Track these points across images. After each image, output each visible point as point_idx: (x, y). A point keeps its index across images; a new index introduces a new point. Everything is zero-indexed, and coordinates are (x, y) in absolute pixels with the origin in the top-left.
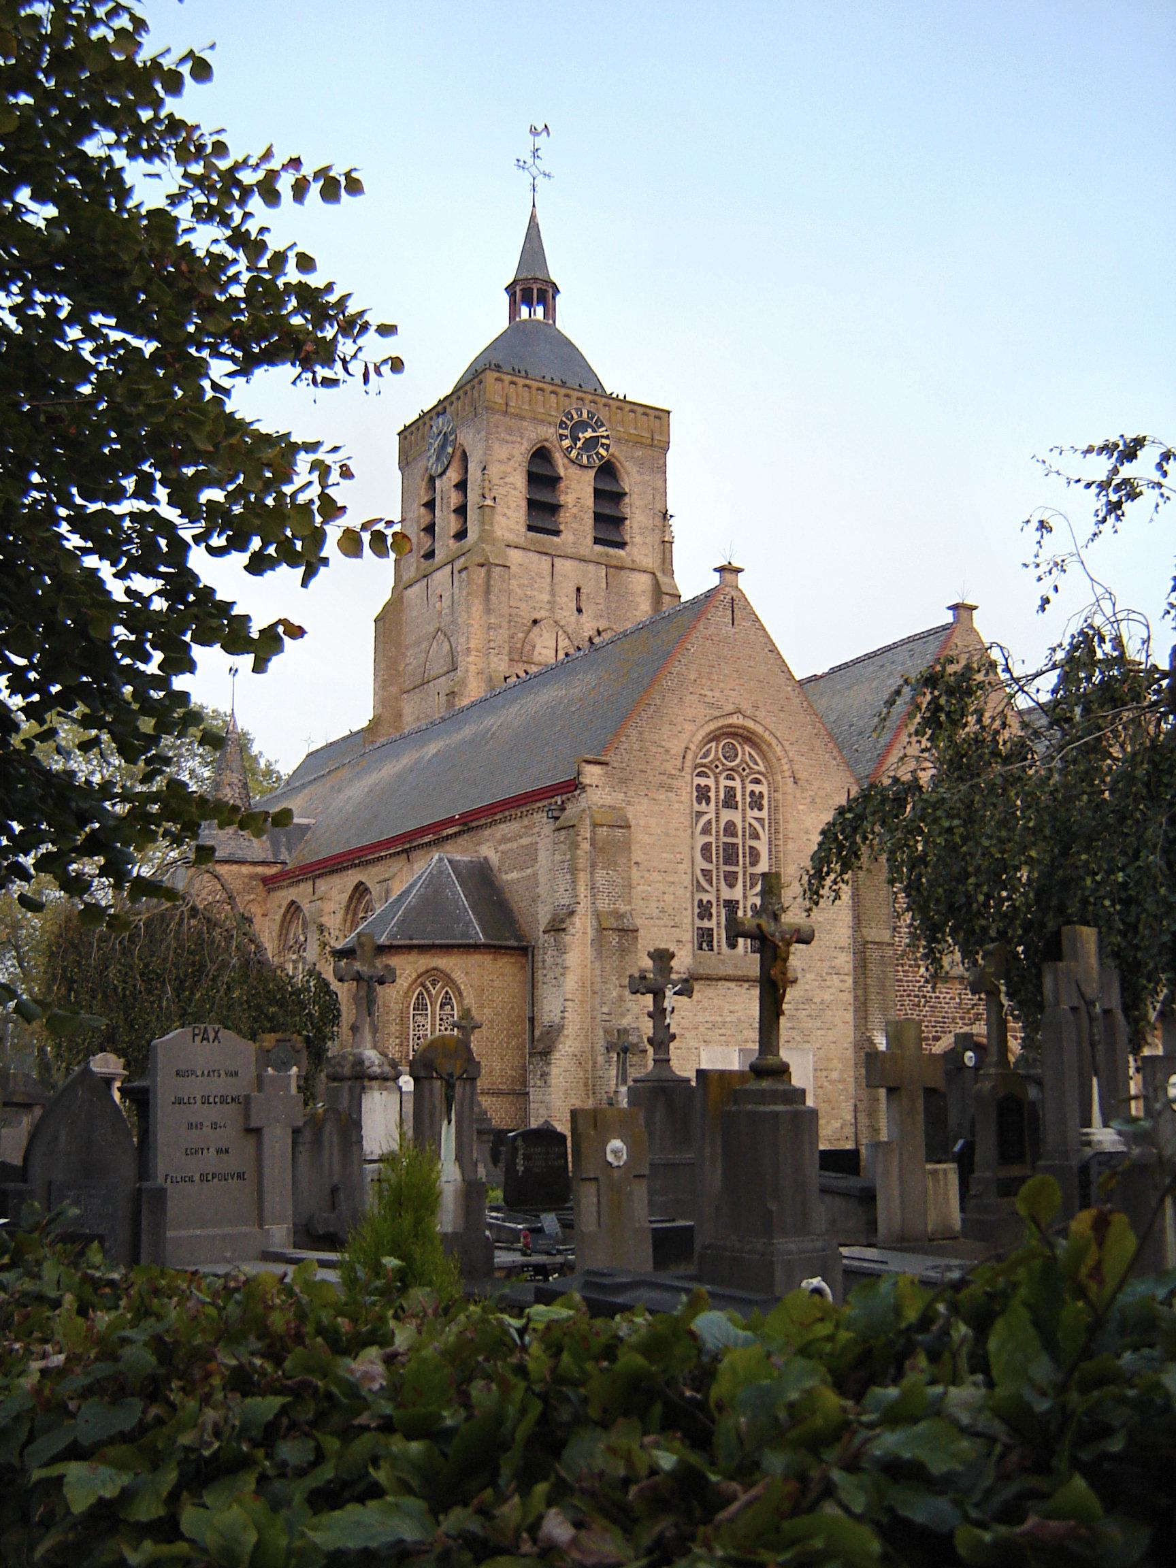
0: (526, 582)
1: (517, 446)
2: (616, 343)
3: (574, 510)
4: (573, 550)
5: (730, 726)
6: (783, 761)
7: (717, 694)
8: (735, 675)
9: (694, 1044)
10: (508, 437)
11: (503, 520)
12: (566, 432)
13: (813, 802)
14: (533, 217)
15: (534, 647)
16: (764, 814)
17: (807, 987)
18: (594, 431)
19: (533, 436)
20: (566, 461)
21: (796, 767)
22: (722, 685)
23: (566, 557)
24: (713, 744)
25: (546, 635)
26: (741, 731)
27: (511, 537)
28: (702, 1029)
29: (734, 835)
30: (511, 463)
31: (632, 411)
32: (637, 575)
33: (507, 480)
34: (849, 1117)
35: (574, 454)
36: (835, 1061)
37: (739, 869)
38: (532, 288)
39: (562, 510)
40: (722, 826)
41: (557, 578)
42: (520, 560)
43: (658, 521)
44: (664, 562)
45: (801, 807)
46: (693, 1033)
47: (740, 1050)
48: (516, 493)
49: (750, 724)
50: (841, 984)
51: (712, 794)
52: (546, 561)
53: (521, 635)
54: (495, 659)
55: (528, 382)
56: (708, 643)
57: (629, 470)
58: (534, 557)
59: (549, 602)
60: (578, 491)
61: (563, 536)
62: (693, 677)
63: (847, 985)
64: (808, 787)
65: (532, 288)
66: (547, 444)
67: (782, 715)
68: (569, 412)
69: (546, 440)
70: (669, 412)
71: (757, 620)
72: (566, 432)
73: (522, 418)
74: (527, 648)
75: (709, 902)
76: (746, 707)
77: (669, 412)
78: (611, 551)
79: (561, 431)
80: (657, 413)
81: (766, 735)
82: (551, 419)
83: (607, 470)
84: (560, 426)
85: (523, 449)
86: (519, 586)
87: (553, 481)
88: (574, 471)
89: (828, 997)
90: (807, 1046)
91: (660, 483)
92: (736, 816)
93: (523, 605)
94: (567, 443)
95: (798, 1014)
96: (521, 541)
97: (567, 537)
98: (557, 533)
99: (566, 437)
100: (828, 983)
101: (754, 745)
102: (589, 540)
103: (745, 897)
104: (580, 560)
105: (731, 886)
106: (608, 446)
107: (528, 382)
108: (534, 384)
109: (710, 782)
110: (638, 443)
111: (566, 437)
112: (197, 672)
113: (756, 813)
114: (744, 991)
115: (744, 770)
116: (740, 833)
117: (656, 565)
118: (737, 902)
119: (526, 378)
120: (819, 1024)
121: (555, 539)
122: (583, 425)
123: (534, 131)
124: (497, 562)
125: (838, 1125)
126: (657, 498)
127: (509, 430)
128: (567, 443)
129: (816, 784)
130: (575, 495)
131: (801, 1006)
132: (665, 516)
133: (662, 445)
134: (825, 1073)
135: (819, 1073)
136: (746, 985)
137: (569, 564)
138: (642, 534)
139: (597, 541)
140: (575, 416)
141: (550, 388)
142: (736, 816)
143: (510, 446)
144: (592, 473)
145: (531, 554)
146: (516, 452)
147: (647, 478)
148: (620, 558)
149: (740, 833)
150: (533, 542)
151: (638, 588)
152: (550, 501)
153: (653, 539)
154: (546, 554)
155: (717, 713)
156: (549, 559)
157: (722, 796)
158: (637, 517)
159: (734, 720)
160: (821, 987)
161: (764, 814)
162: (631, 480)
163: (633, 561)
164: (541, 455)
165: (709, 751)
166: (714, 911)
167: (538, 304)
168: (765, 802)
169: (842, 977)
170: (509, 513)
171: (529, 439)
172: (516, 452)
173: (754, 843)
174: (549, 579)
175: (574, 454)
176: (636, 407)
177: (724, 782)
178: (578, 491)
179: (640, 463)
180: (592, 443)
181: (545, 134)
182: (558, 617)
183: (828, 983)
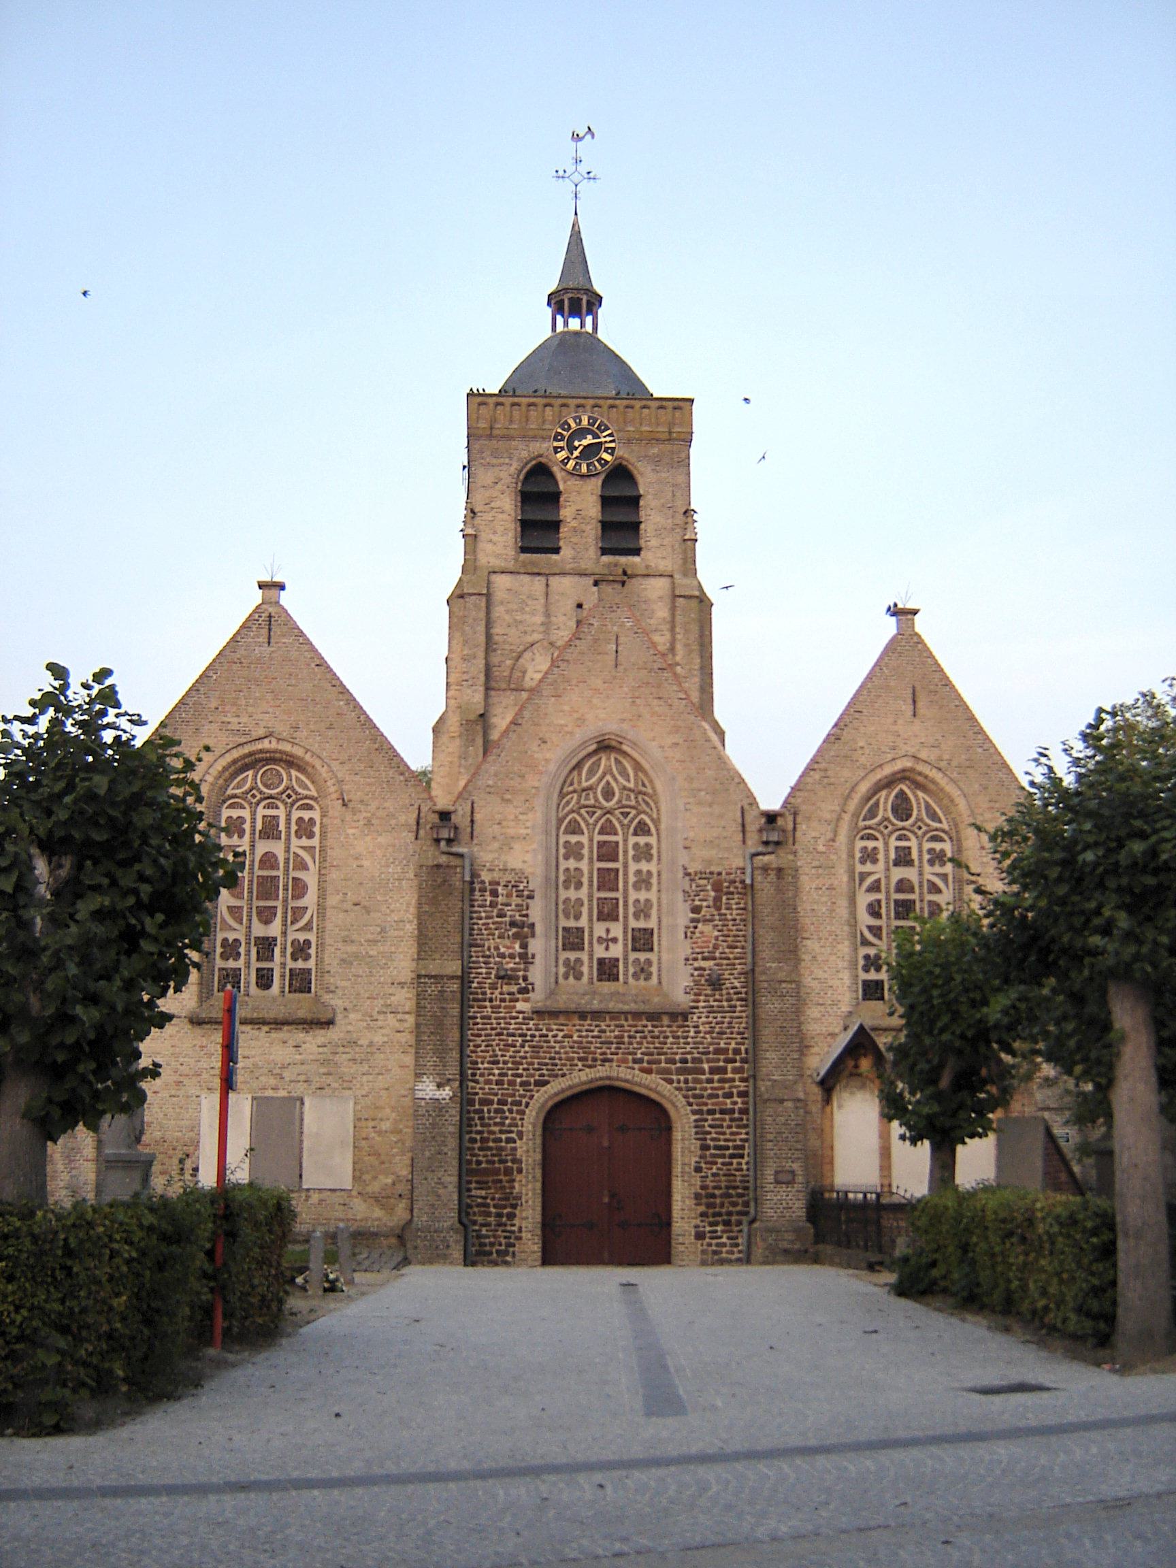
0: (515, 607)
1: (505, 467)
2: (644, 337)
3: (574, 524)
4: (572, 566)
5: (261, 751)
6: (329, 783)
7: (244, 720)
8: (269, 697)
9: (193, 1091)
10: (495, 461)
11: (489, 547)
12: (561, 444)
13: (369, 823)
14: (575, 225)
15: (524, 672)
16: (315, 842)
17: (350, 1028)
18: (596, 436)
19: (524, 454)
20: (564, 473)
21: (345, 788)
22: (250, 709)
23: (563, 574)
24: (250, 773)
25: (538, 658)
26: (278, 755)
27: (497, 563)
28: (205, 1076)
29: (274, 866)
30: (499, 486)
31: (661, 407)
32: (653, 582)
33: (493, 505)
34: (405, 1172)
35: (571, 464)
36: (388, 1111)
37: (279, 904)
38: (574, 298)
39: (562, 525)
40: (257, 859)
41: (553, 598)
42: (508, 585)
43: (680, 519)
44: (685, 560)
45: (351, 831)
46: (195, 1080)
47: (254, 1099)
48: (504, 516)
49: (287, 747)
50: (397, 1025)
51: (247, 827)
52: (539, 582)
53: (509, 662)
54: (469, 691)
55: (516, 400)
56: (235, 667)
57: (642, 469)
58: (526, 579)
59: (543, 624)
60: (581, 504)
61: (562, 553)
62: (213, 705)
63: (407, 1025)
64: (362, 808)
65: (574, 298)
66: (543, 460)
67: (330, 733)
68: (566, 423)
69: (541, 456)
70: (692, 401)
71: (302, 634)
72: (561, 444)
73: (509, 438)
74: (517, 674)
75: (236, 940)
76: (283, 729)
77: (692, 401)
78: (623, 560)
79: (556, 444)
80: (676, 403)
81: (308, 757)
82: (544, 433)
83: (620, 474)
84: (555, 439)
85: (512, 470)
86: (507, 612)
87: (553, 498)
88: (574, 483)
89: (378, 1039)
90: (347, 1092)
91: (681, 479)
92: (277, 848)
93: (512, 632)
94: (562, 455)
95: (337, 1058)
96: (511, 565)
97: (566, 552)
98: (557, 550)
99: (562, 448)
100: (380, 1023)
101: (300, 769)
102: (593, 552)
103: (284, 933)
104: (581, 575)
105: (267, 922)
106: (613, 449)
107: (516, 400)
108: (524, 401)
109: (246, 813)
110: (653, 439)
111: (562, 448)
112: (1096, 707)
113: (305, 842)
114: (263, 1034)
115: (289, 796)
116: (281, 865)
117: (676, 567)
118: (275, 939)
119: (514, 395)
120: (366, 1068)
121: (554, 557)
122: (581, 433)
123: (577, 138)
124: (471, 591)
125: (389, 1181)
126: (678, 494)
127: (495, 453)
128: (562, 455)
129: (374, 805)
130: (574, 508)
131: (341, 1049)
132: (689, 512)
133: (683, 436)
134: (371, 1124)
135: (363, 1123)
136: (266, 1028)
137: (567, 581)
138: (657, 536)
139: (604, 551)
140: (573, 425)
141: (544, 401)
142: (277, 848)
143: (496, 469)
144: (597, 483)
145: (522, 577)
146: (503, 475)
147: (664, 475)
148: (634, 565)
149: (281, 865)
150: (524, 564)
151: (653, 595)
152: (550, 518)
153: (672, 539)
154: (539, 574)
155: (243, 740)
156: (543, 579)
157: (259, 826)
158: (652, 518)
159: (265, 744)
160: (368, 1027)
161: (315, 842)
162: (647, 480)
163: (647, 567)
164: (539, 472)
165: (245, 780)
166: (242, 950)
167: (588, 314)
168: (317, 829)
169: (399, 1016)
170: (495, 538)
171: (519, 459)
172: (503, 475)
173: (298, 874)
174: (543, 601)
175: (571, 464)
176: (664, 403)
177: (261, 811)
178: (581, 504)
179: (657, 461)
180: (590, 452)
181: (589, 137)
182: (553, 638)
183: (380, 1023)
